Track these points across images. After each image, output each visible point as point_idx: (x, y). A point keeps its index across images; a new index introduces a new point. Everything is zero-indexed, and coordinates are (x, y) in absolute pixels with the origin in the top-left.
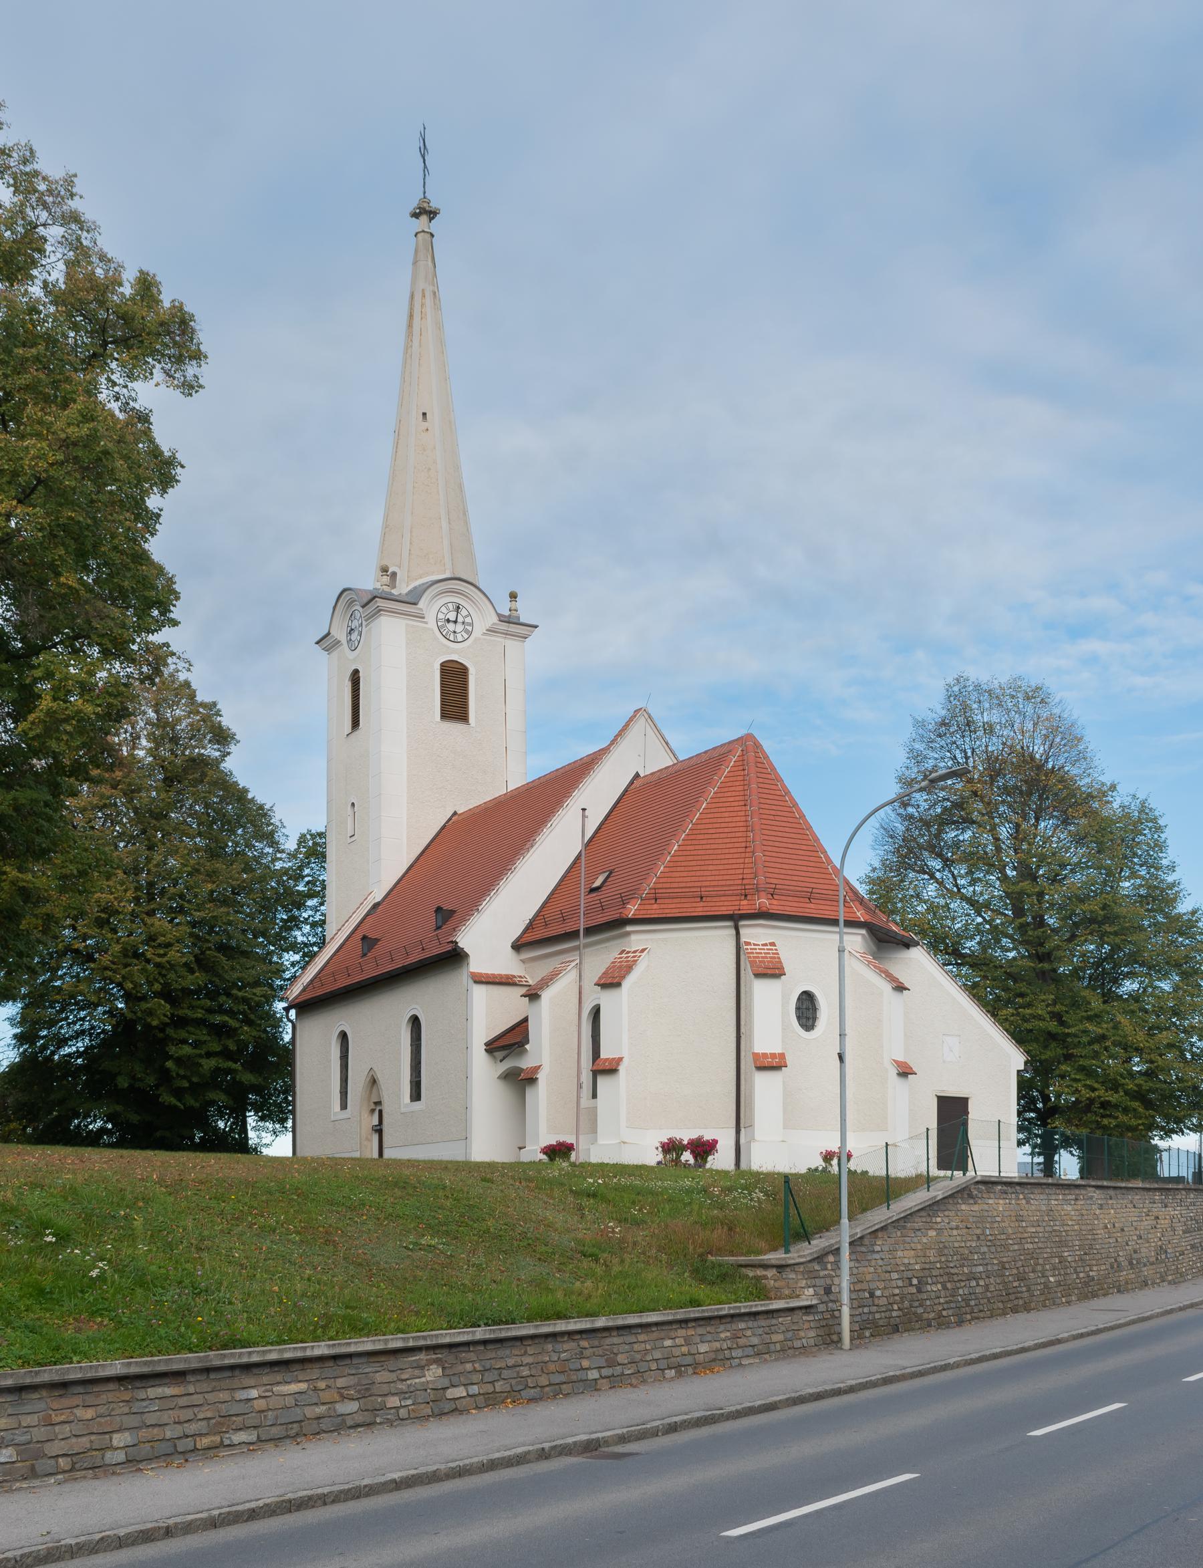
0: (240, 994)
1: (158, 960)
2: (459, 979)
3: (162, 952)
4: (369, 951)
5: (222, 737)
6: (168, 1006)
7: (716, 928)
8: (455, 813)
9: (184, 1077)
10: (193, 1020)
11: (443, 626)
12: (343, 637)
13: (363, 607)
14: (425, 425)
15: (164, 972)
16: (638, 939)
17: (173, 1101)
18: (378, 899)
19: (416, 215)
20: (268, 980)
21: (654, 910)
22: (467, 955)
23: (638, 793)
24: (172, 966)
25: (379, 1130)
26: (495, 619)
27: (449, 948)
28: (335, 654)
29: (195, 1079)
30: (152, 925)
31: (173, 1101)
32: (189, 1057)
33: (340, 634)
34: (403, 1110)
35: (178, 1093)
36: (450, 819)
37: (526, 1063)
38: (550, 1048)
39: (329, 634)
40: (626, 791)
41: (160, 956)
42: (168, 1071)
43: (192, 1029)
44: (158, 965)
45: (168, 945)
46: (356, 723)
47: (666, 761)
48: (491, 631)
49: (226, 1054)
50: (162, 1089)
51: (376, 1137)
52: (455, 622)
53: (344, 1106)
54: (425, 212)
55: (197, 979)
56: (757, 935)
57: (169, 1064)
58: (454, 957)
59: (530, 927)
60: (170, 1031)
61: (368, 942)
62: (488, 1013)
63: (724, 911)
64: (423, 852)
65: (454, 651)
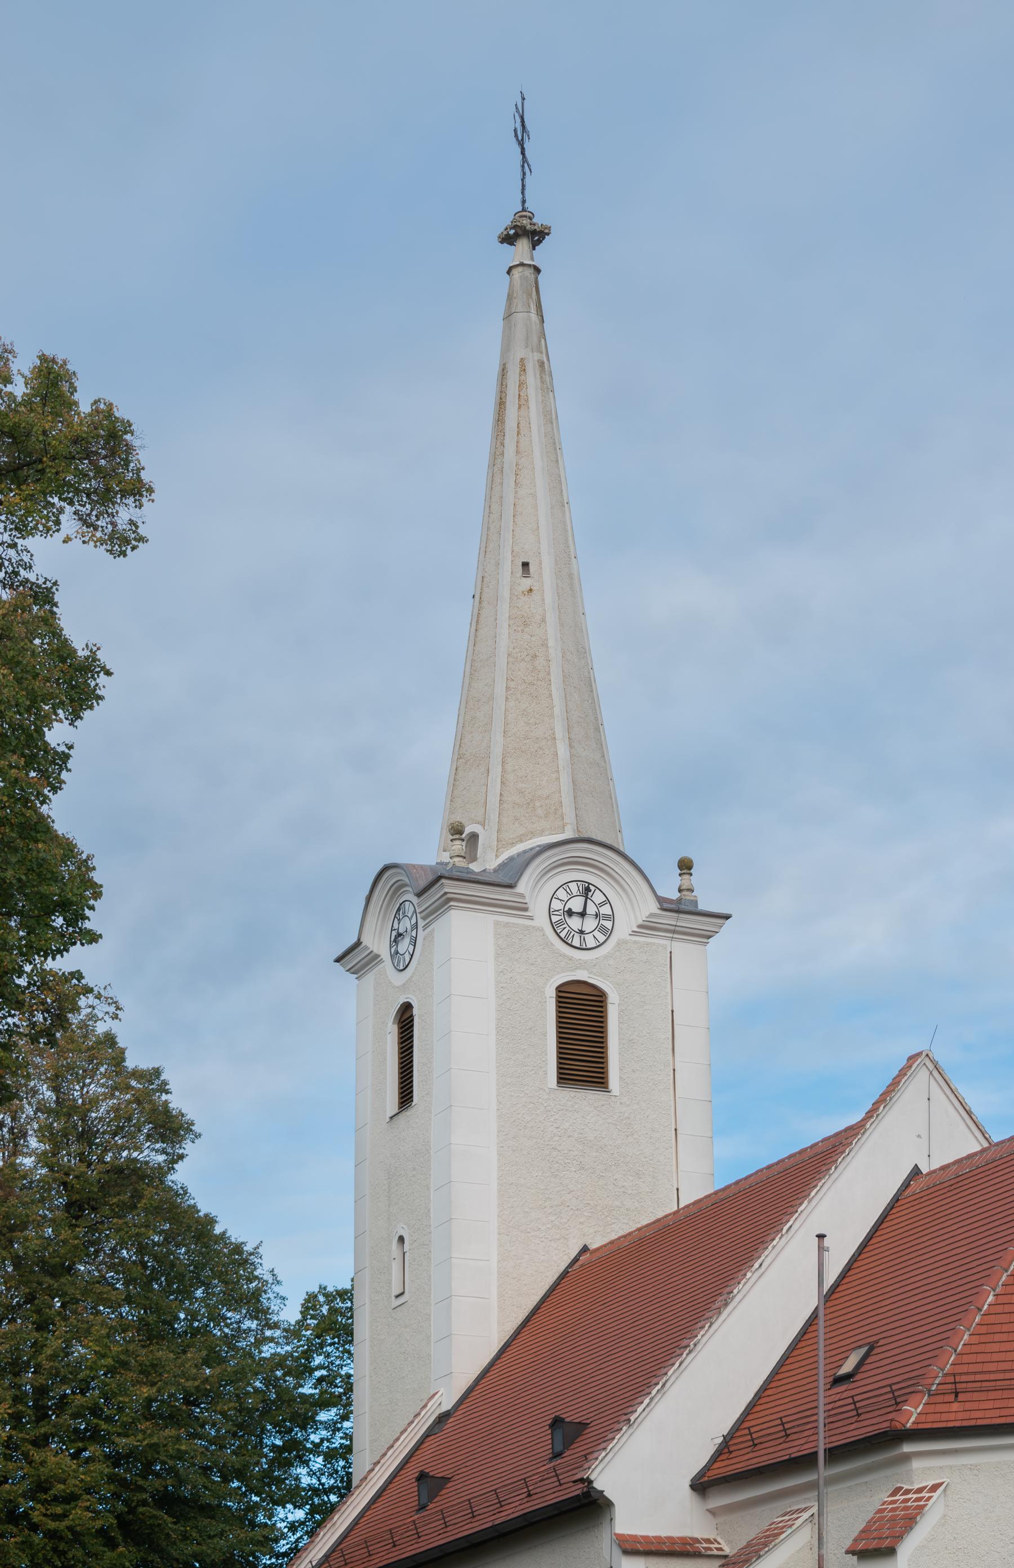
3: (59, 1510)
5: (171, 1129)
8: (585, 1249)
11: (560, 923)
13: (419, 895)
14: (526, 583)
15: (62, 1546)
16: (925, 1467)
19: (508, 239)
21: (955, 1414)
22: (609, 1504)
23: (919, 1204)
26: (653, 907)
27: (577, 1490)
28: (370, 978)
33: (377, 942)
36: (576, 1260)
39: (358, 943)
41: (55, 1517)
44: (52, 1535)
45: (71, 1498)
46: (406, 1096)
48: (647, 927)
52: (583, 914)
54: (525, 232)
58: (589, 1507)
59: (725, 1449)
61: (430, 1484)
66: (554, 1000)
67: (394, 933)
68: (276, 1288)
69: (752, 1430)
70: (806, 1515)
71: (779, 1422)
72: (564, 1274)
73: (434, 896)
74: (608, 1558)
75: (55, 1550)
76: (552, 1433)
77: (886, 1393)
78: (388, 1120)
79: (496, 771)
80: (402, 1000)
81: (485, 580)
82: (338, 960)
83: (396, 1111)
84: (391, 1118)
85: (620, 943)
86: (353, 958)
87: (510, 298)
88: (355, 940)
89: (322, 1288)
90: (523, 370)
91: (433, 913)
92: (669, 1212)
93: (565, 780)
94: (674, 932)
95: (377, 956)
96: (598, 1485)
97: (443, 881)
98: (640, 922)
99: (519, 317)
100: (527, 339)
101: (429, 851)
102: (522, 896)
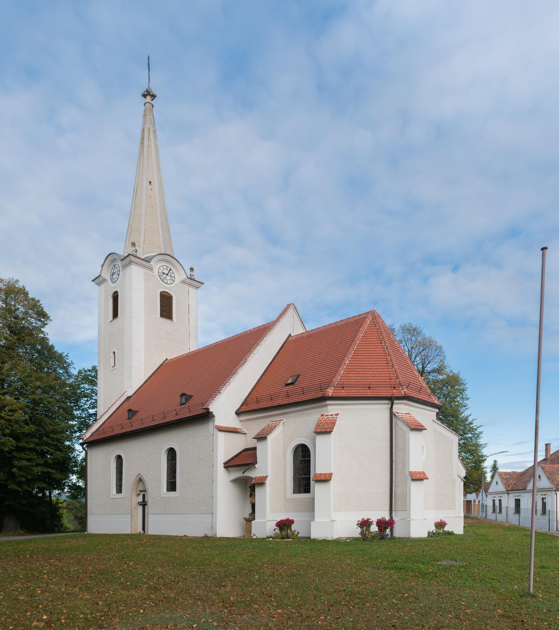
0: (55, 436)
2: (210, 428)
3: (10, 413)
4: (133, 417)
5: (42, 315)
6: (14, 441)
7: (378, 404)
8: (167, 359)
9: (23, 476)
10: (27, 448)
12: (108, 277)
13: (122, 260)
14: (150, 187)
15: (12, 424)
16: (332, 408)
17: (16, 487)
18: (129, 395)
19: (144, 96)
20: (67, 432)
21: (343, 393)
22: (213, 416)
23: (290, 345)
24: (17, 422)
25: (144, 504)
26: (185, 277)
27: (204, 411)
28: (103, 286)
29: (29, 477)
30: (5, 399)
31: (16, 487)
32: (26, 466)
33: (106, 275)
34: (162, 496)
35: (19, 484)
36: (164, 362)
37: (254, 474)
38: (275, 464)
39: (100, 276)
40: (285, 342)
41: (9, 416)
42: (13, 473)
43: (27, 453)
44: (9, 420)
45: (15, 411)
46: (115, 314)
47: (302, 331)
48: (183, 282)
49: (46, 465)
50: (9, 482)
51: (140, 508)
52: (167, 275)
53: (119, 490)
54: (148, 94)
56: (401, 408)
57: (14, 470)
58: (206, 416)
59: (245, 403)
60: (15, 454)
61: (131, 413)
62: (226, 447)
63: (384, 394)
68: (73, 365)
70: (282, 422)
72: (161, 365)
73: (127, 260)
74: (212, 432)
75: (9, 425)
79: (142, 234)
82: (93, 281)
85: (176, 284)
86: (98, 280)
87: (145, 111)
89: (83, 369)
90: (149, 130)
91: (125, 267)
93: (161, 240)
96: (211, 410)
99: (148, 116)
101: (122, 252)
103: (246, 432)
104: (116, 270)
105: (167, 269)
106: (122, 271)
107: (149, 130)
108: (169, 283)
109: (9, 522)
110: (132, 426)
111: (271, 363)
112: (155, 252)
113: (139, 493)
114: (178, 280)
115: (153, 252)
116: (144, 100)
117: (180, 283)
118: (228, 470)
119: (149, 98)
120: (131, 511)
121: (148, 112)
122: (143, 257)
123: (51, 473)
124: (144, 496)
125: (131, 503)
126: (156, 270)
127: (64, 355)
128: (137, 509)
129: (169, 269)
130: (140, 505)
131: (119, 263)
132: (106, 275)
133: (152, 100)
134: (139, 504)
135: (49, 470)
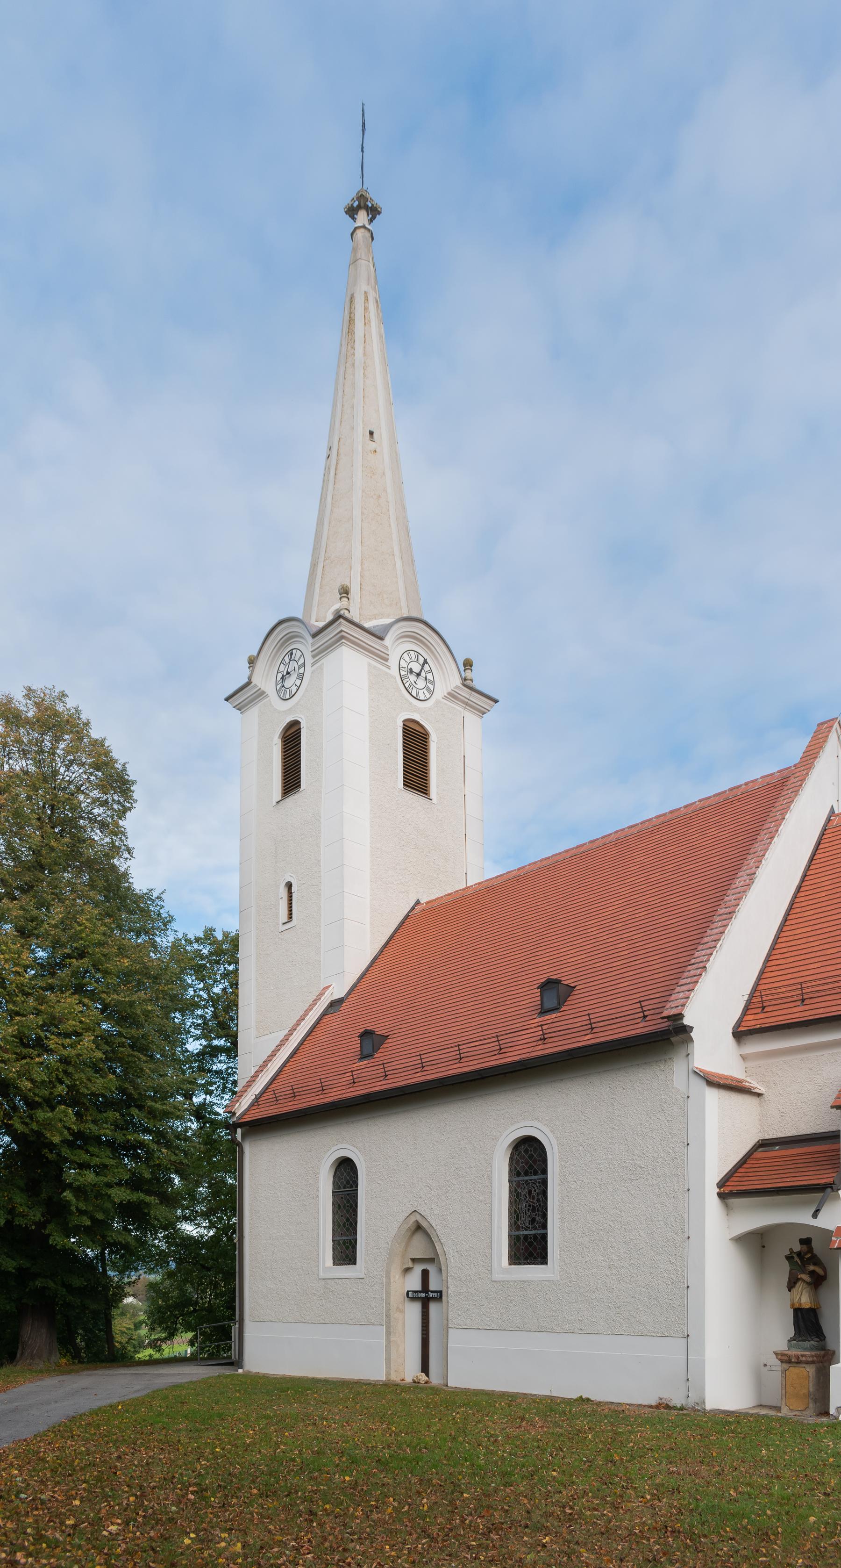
1: (65, 1053)
2: (674, 1074)
5: (118, 784)
8: (418, 903)
13: (314, 636)
14: (372, 446)
25: (426, 1298)
28: (254, 712)
33: (265, 680)
34: (497, 1276)
36: (413, 909)
39: (249, 683)
46: (291, 781)
48: (452, 696)
51: (414, 1310)
52: (418, 675)
53: (346, 1251)
55: (104, 1085)
57: (68, 1195)
64: (387, 943)
65: (416, 710)
66: (401, 729)
67: (280, 676)
69: (591, 1016)
71: (587, 1017)
72: (407, 917)
74: (682, 1088)
76: (542, 996)
77: (835, 982)
78: (274, 803)
79: (357, 567)
80: (289, 719)
81: (342, 440)
83: (280, 798)
84: (278, 802)
86: (242, 697)
88: (247, 680)
90: (366, 299)
91: (319, 653)
92: (458, 888)
94: (467, 704)
95: (263, 693)
97: (341, 620)
98: (450, 690)
100: (369, 279)
102: (386, 648)
103: (761, 1089)
104: (293, 664)
105: (417, 661)
106: (313, 664)
107: (366, 299)
108: (422, 697)
109: (35, 1335)
110: (368, 1077)
111: (799, 889)
112: (388, 616)
113: (410, 1265)
114: (441, 690)
115: (382, 616)
116: (350, 224)
117: (445, 698)
118: (727, 1206)
119: (362, 217)
120: (388, 1316)
121: (362, 253)
122: (367, 625)
123: (148, 1205)
124: (425, 1274)
125: (388, 1294)
126: (393, 661)
127: (155, 894)
128: (402, 1311)
129: (422, 661)
130: (413, 1299)
131: (306, 647)
132: (265, 680)
133: (371, 221)
134: (411, 1296)
135: (142, 1196)
